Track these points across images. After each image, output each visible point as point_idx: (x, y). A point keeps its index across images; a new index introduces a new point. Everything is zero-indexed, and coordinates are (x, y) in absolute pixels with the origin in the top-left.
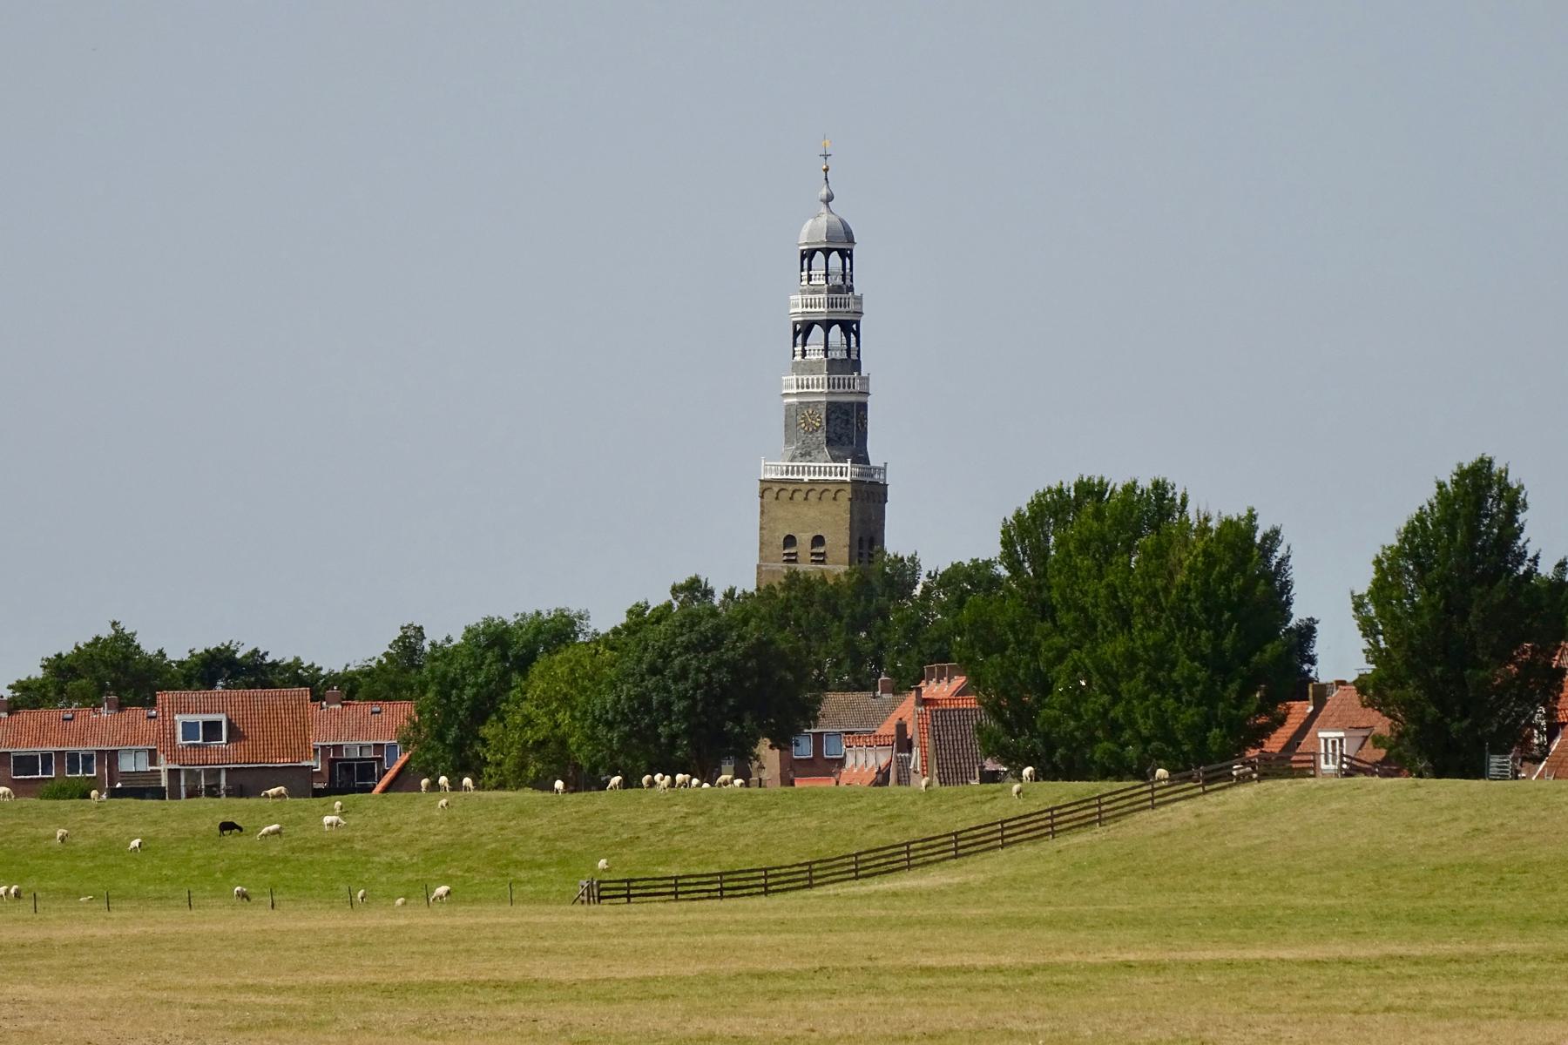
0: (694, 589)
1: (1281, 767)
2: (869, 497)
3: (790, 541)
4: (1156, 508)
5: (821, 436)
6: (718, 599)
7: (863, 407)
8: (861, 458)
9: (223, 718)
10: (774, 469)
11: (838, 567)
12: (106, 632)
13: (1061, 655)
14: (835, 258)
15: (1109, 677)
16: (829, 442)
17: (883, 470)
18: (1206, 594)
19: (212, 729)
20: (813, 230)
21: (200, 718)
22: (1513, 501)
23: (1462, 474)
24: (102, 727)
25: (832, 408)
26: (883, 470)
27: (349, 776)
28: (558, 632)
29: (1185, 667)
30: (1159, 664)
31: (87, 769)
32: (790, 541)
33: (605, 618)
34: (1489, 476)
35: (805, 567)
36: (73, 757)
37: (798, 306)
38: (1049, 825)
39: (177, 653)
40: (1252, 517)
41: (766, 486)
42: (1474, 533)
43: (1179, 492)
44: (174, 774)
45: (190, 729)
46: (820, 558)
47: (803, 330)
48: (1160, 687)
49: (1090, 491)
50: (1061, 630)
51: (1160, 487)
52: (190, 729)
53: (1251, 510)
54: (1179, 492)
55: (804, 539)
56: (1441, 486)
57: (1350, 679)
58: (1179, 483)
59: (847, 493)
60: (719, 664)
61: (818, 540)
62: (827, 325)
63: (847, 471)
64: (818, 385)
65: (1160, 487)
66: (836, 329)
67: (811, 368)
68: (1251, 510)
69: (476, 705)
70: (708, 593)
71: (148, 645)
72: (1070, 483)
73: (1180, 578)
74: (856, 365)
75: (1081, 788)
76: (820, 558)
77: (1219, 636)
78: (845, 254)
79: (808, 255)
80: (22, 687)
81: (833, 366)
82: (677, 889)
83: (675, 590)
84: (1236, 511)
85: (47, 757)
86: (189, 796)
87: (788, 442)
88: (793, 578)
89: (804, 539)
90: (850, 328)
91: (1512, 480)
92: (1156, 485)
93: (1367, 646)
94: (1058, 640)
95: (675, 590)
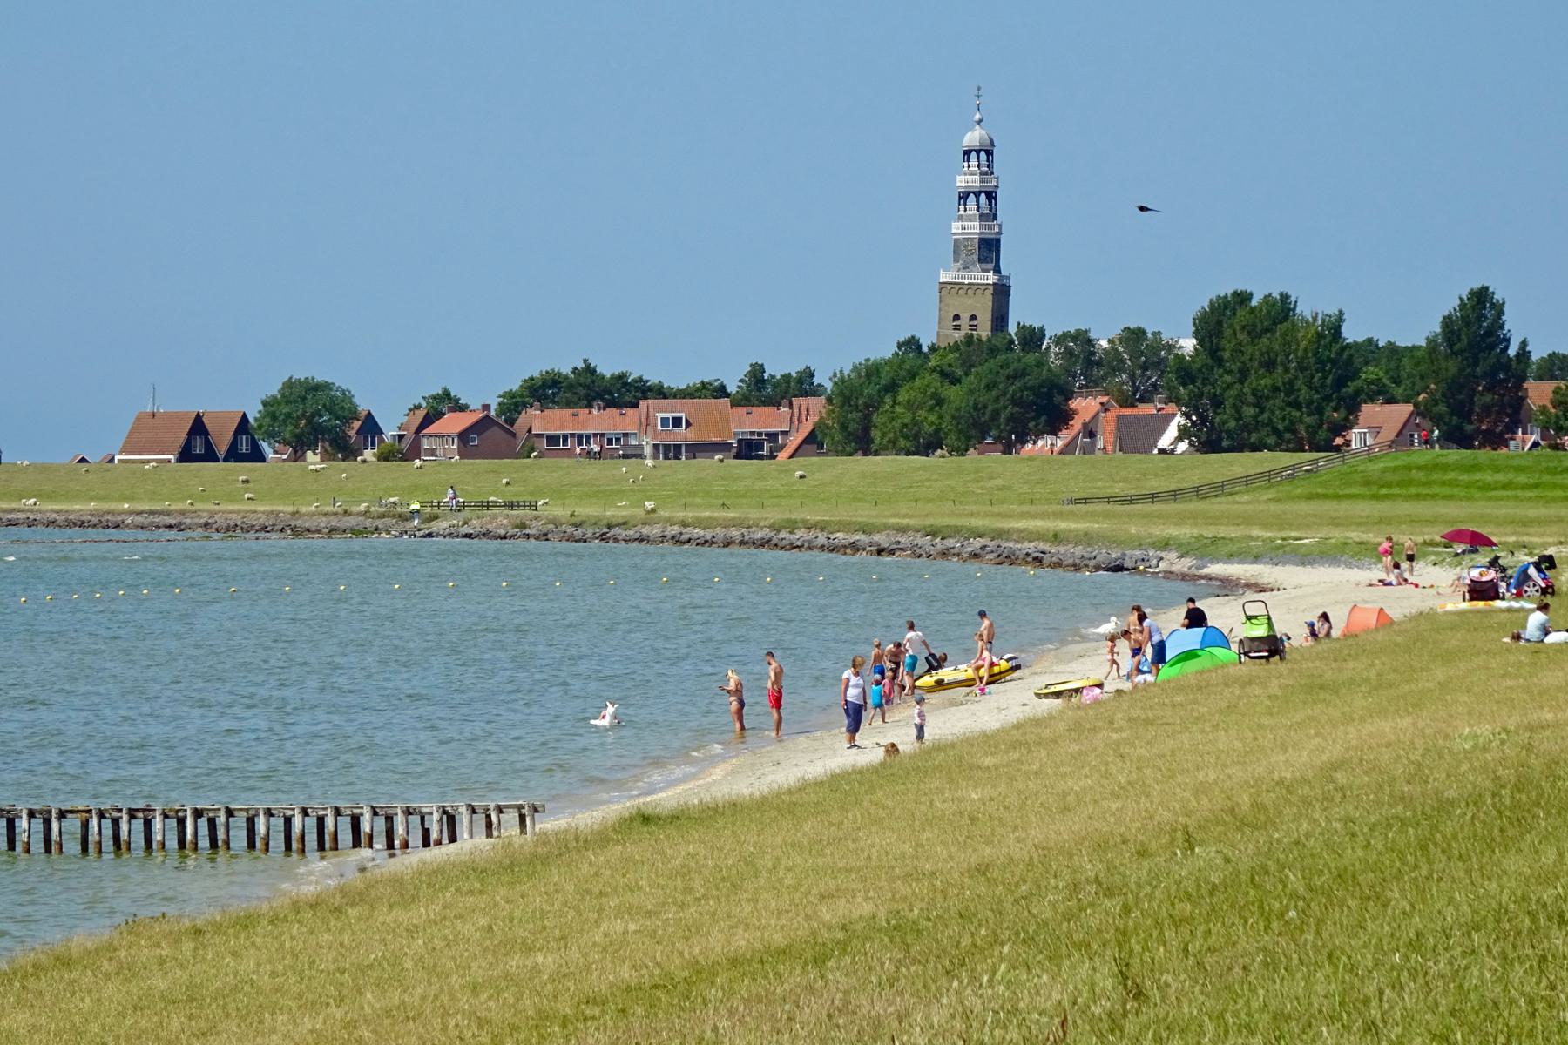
2: (1002, 292)
3: (957, 317)
5: (976, 257)
8: (997, 271)
10: (946, 277)
11: (984, 331)
12: (581, 365)
13: (1229, 386)
14: (983, 155)
15: (1260, 402)
19: (677, 422)
20: (973, 138)
21: (670, 415)
22: (1499, 309)
23: (1473, 293)
24: (599, 420)
26: (1008, 278)
29: (1304, 394)
31: (565, 443)
32: (957, 317)
36: (580, 436)
37: (962, 182)
38: (1292, 475)
39: (677, 380)
41: (943, 285)
43: (1293, 299)
45: (664, 421)
47: (964, 197)
50: (1229, 372)
51: (1285, 297)
53: (1341, 313)
55: (965, 316)
61: (973, 318)
62: (977, 194)
63: (992, 278)
64: (974, 228)
65: (1285, 297)
66: (983, 196)
68: (1341, 313)
69: (868, 413)
70: (919, 347)
72: (1230, 291)
73: (1303, 344)
74: (995, 217)
77: (1325, 378)
78: (989, 153)
79: (967, 153)
81: (982, 217)
85: (565, 437)
87: (956, 261)
89: (965, 316)
90: (991, 196)
93: (846, 373)
94: (1228, 378)
95: (900, 346)
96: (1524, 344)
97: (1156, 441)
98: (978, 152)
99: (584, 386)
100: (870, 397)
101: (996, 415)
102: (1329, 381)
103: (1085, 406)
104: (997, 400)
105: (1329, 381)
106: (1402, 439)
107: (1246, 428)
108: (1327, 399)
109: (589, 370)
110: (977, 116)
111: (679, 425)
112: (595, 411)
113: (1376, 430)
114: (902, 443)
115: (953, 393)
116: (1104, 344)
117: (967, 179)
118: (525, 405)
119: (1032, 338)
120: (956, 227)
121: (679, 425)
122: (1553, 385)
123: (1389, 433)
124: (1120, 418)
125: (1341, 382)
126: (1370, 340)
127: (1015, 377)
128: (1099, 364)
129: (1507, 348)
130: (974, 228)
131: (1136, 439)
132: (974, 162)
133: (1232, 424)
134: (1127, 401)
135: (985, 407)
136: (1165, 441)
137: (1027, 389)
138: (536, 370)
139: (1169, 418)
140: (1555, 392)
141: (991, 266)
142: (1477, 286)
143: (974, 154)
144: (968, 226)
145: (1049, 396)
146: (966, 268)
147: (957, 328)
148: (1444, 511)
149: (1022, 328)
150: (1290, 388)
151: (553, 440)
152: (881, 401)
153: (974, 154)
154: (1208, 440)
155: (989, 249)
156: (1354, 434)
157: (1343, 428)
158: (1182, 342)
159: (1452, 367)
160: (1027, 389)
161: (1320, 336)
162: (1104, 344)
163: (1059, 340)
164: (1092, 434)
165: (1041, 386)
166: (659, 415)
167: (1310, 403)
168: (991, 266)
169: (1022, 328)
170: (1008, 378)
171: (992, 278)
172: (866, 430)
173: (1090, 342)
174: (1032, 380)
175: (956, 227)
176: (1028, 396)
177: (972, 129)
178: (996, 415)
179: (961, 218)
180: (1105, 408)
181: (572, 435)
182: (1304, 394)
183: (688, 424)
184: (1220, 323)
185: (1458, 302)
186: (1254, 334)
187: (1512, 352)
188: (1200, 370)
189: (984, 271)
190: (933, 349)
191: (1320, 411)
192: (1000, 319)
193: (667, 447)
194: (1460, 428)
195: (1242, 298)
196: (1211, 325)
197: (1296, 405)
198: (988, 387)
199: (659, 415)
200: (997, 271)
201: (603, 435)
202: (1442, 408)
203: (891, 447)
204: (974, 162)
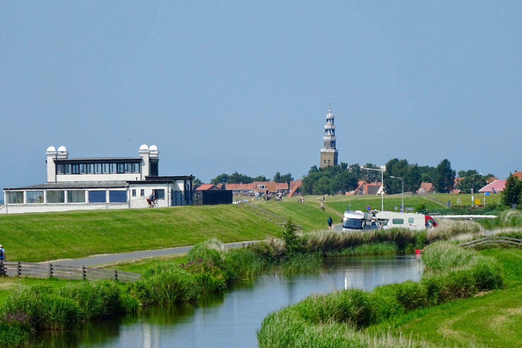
2: (336, 154)
8: (335, 149)
10: (322, 150)
11: (332, 164)
12: (235, 173)
14: (331, 131)
19: (263, 187)
20: (329, 116)
32: (325, 160)
47: (327, 130)
51: (405, 160)
55: (327, 160)
59: (333, 154)
62: (330, 130)
63: (334, 151)
65: (405, 160)
67: (328, 136)
74: (334, 136)
78: (333, 120)
79: (327, 120)
81: (331, 136)
83: (312, 168)
86: (384, 210)
89: (327, 160)
90: (333, 130)
95: (312, 168)
97: (144, 211)
99: (236, 178)
101: (342, 185)
103: (361, 183)
106: (431, 191)
108: (414, 182)
109: (237, 174)
113: (425, 189)
114: (320, 192)
115: (330, 180)
116: (362, 167)
117: (328, 126)
118: (218, 183)
119: (344, 166)
120: (325, 138)
123: (428, 189)
124: (369, 186)
125: (417, 179)
126: (427, 166)
127: (346, 177)
128: (361, 172)
130: (329, 138)
131: (373, 191)
132: (329, 122)
133: (394, 188)
134: (369, 182)
136: (379, 192)
138: (220, 173)
139: (379, 187)
142: (445, 159)
144: (327, 138)
146: (327, 148)
147: (325, 163)
149: (342, 163)
152: (314, 183)
154: (389, 191)
155: (333, 143)
156: (420, 190)
157: (417, 189)
158: (381, 167)
159: (439, 176)
161: (413, 169)
162: (362, 167)
163: (351, 167)
164: (362, 190)
166: (259, 186)
167: (411, 183)
169: (342, 163)
171: (334, 151)
172: (311, 189)
173: (359, 167)
178: (342, 185)
179: (326, 136)
180: (365, 183)
182: (410, 181)
184: (391, 166)
186: (399, 168)
190: (320, 169)
191: (413, 185)
192: (336, 161)
195: (396, 160)
196: (390, 165)
197: (408, 183)
198: (340, 179)
199: (259, 186)
200: (335, 149)
202: (438, 184)
203: (318, 194)
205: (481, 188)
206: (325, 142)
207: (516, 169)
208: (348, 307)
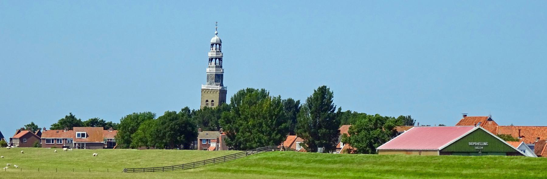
0: (187, 109)
1: (193, 148)
3: (207, 101)
4: (264, 94)
5: (214, 80)
6: (191, 112)
7: (222, 75)
8: (222, 85)
9: (85, 133)
10: (204, 87)
12: (69, 115)
14: (218, 45)
16: (215, 82)
17: (226, 88)
18: (270, 112)
19: (83, 135)
20: (214, 40)
21: (81, 133)
24: (65, 134)
25: (216, 75)
26: (226, 88)
27: (111, 145)
28: (150, 116)
30: (260, 127)
31: (53, 142)
32: (207, 101)
33: (159, 114)
34: (326, 90)
35: (210, 106)
36: (58, 140)
39: (84, 119)
40: (280, 97)
41: (203, 90)
42: (322, 102)
43: (267, 92)
44: (75, 144)
45: (79, 135)
46: (213, 105)
47: (211, 60)
48: (259, 132)
49: (250, 91)
51: (263, 91)
52: (79, 135)
54: (267, 92)
55: (210, 101)
56: (315, 91)
57: (117, 121)
58: (267, 90)
60: (175, 124)
61: (213, 101)
62: (216, 59)
63: (219, 88)
64: (214, 70)
65: (263, 91)
69: (135, 132)
70: (189, 111)
71: (78, 117)
74: (221, 67)
75: (238, 151)
76: (213, 105)
78: (220, 45)
79: (212, 45)
80: (55, 125)
81: (216, 67)
82: (144, 170)
84: (277, 96)
85: (53, 140)
86: (201, 149)
87: (208, 81)
88: (205, 108)
89: (210, 101)
90: (220, 59)
91: (331, 91)
92: (262, 90)
96: (340, 109)
98: (216, 44)
100: (133, 127)
102: (274, 123)
104: (165, 129)
105: (274, 123)
107: (247, 141)
110: (216, 32)
111: (84, 136)
112: (65, 131)
117: (212, 54)
120: (208, 70)
121: (84, 136)
122: (349, 126)
129: (334, 110)
130: (214, 70)
132: (214, 48)
135: (161, 131)
137: (177, 124)
140: (350, 128)
141: (219, 83)
142: (321, 86)
143: (215, 45)
145: (185, 127)
148: (451, 161)
150: (261, 125)
151: (48, 141)
153: (215, 45)
155: (219, 78)
160: (177, 124)
165: (182, 124)
166: (77, 133)
168: (219, 83)
170: (170, 120)
171: (219, 88)
174: (179, 121)
175: (208, 70)
176: (177, 127)
177: (214, 36)
179: (209, 67)
181: (55, 139)
183: (87, 136)
185: (314, 92)
186: (251, 104)
187: (336, 112)
188: (232, 118)
189: (217, 85)
191: (270, 134)
193: (79, 144)
194: (313, 142)
197: (262, 132)
199: (77, 133)
201: (66, 139)
204: (214, 48)
205: (384, 142)
206: (208, 76)
207: (465, 112)
208: (203, 121)
